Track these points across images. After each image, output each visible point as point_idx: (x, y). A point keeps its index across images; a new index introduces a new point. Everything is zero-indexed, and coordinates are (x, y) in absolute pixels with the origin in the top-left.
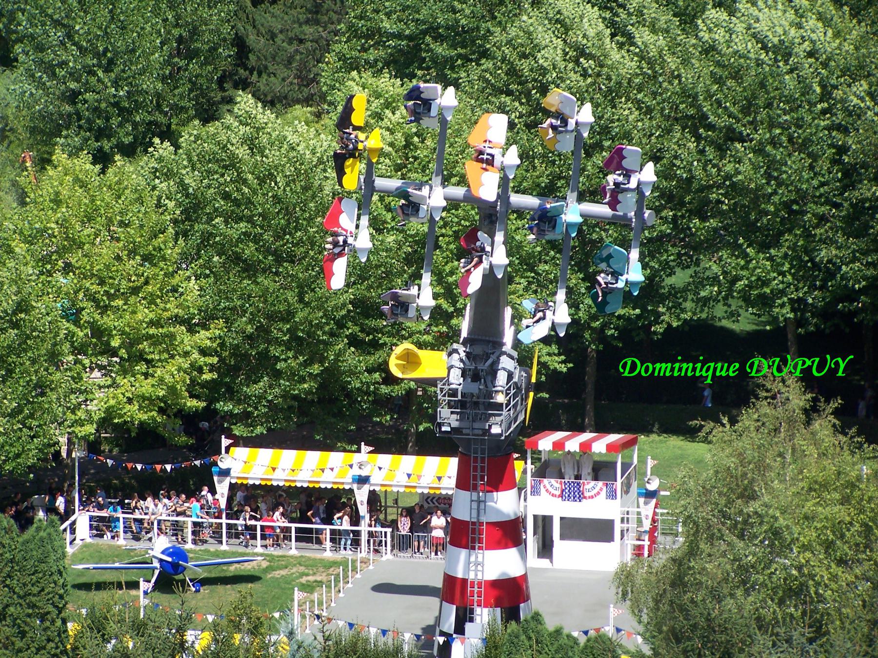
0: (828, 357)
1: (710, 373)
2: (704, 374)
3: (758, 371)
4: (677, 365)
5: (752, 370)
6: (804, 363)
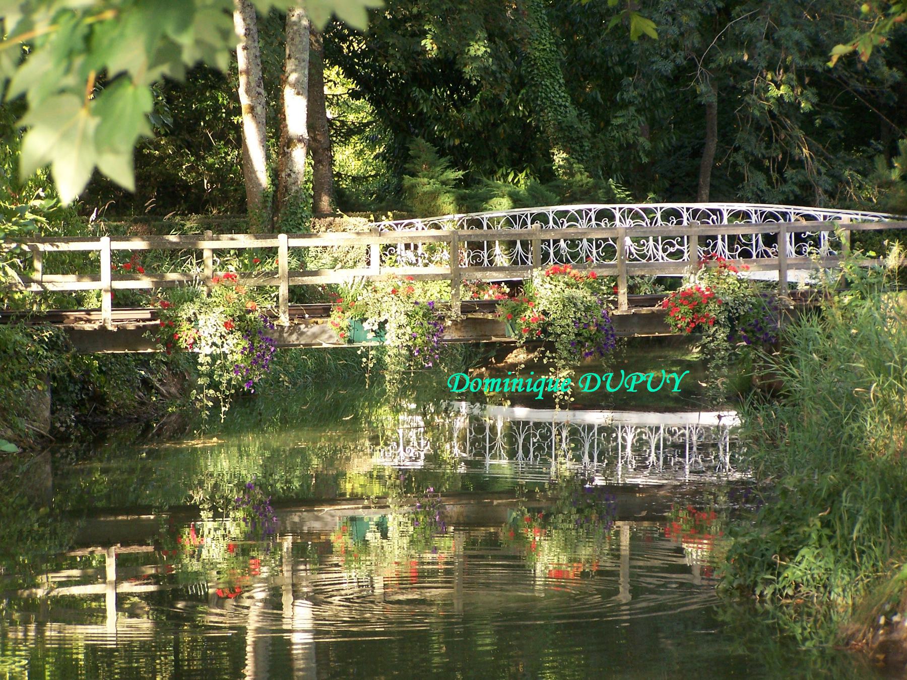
0: (622, 372)
1: (541, 388)
2: (535, 390)
3: (460, 387)
4: (507, 381)
5: (453, 385)
6: (638, 377)
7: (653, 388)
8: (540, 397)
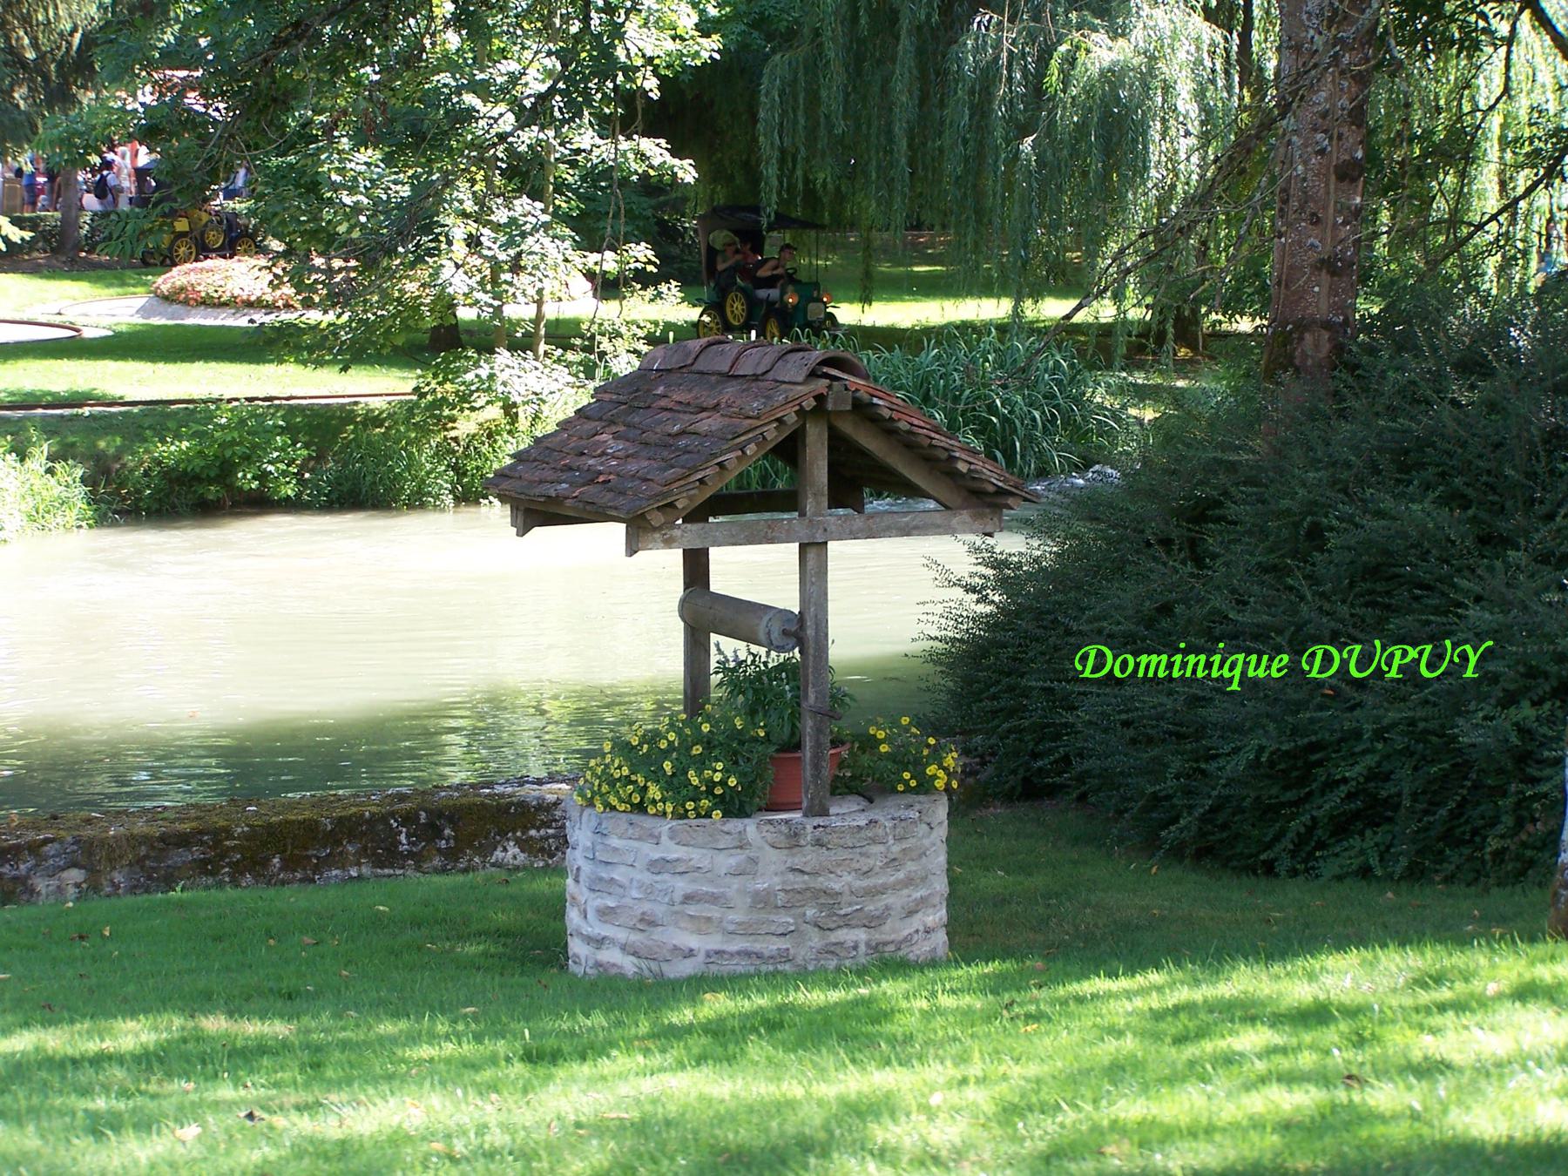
1: (1237, 672)
4: (1178, 658)
6: (1405, 654)
7: (1360, 670)
8: (1235, 687)
